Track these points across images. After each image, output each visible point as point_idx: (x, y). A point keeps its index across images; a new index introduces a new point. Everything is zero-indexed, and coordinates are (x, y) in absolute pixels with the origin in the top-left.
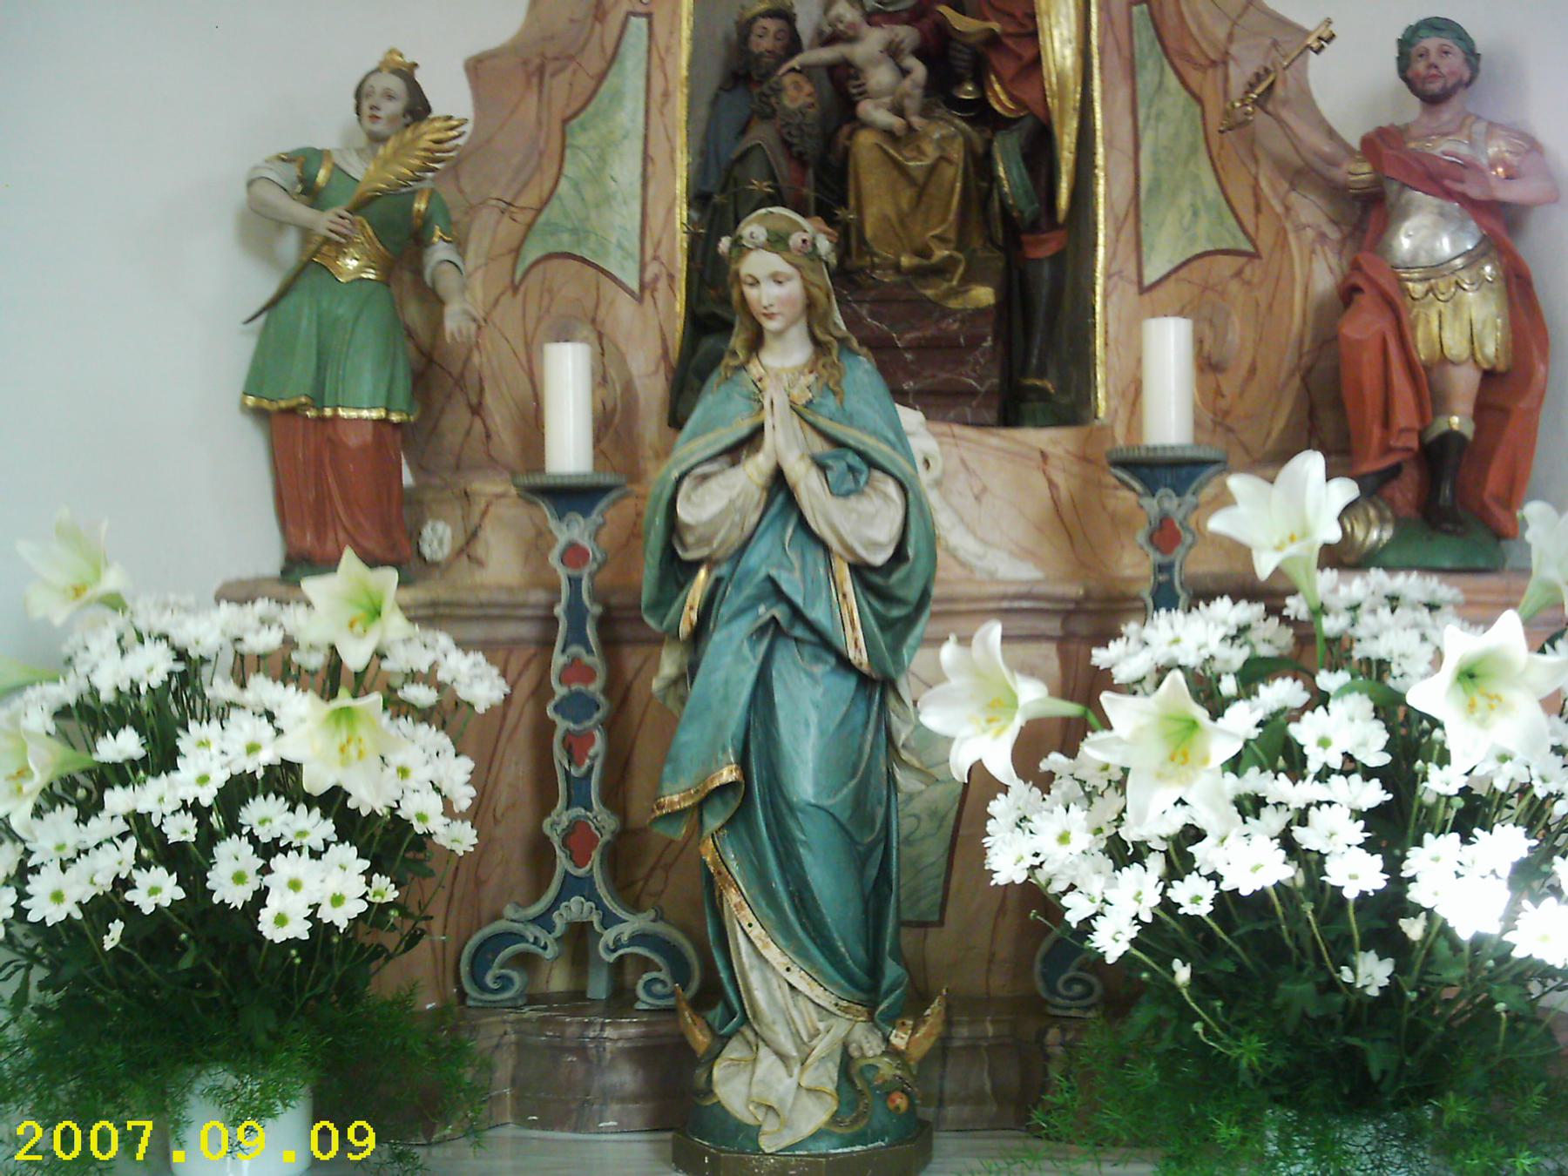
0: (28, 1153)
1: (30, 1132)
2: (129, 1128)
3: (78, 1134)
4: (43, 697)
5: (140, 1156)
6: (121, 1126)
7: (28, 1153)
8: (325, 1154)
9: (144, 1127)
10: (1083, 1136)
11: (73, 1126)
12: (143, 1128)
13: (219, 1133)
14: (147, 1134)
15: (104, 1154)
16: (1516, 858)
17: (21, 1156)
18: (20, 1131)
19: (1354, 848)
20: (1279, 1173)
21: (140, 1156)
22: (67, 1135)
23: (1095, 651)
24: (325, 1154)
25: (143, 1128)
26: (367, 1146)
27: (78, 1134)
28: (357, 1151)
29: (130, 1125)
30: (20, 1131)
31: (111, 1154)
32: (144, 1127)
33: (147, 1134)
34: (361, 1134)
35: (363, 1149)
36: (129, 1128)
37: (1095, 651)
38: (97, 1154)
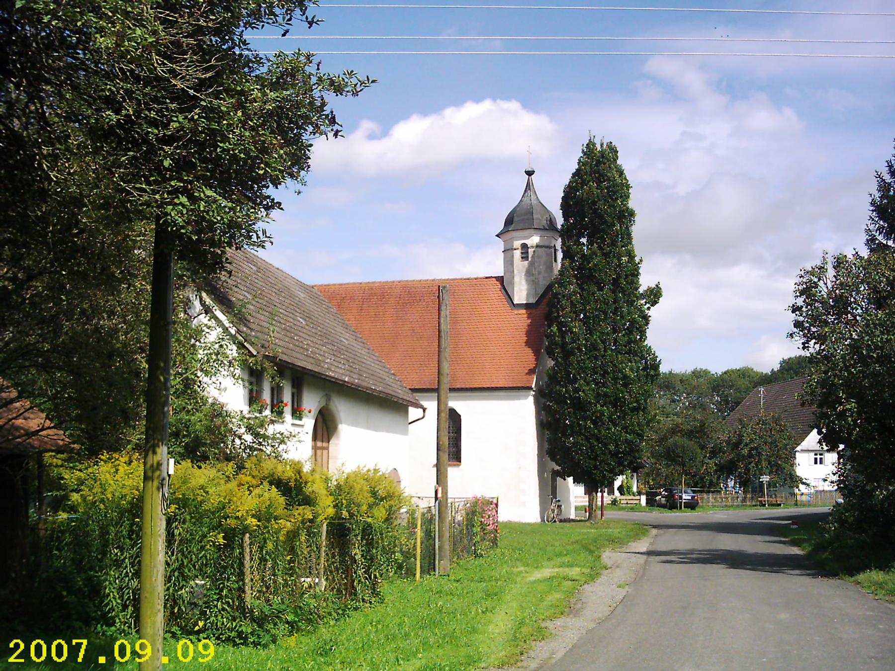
0: (16, 658)
1: (17, 646)
2: (74, 644)
3: (44, 647)
4: (140, 406)
5: (80, 660)
6: (69, 643)
7: (16, 658)
8: (38, 658)
9: (82, 643)
10: (303, 635)
11: (42, 642)
12: (82, 643)
13: (188, 647)
14: (84, 647)
15: (122, 658)
16: (709, 369)
17: (12, 660)
18: (12, 645)
19: (602, 138)
20: (470, 670)
21: (80, 660)
22: (38, 648)
23: (572, 478)
24: (38, 658)
25: (82, 643)
26: (209, 654)
27: (44, 647)
28: (203, 657)
29: (74, 642)
30: (12, 645)
31: (126, 659)
32: (82, 643)
33: (84, 647)
34: (206, 647)
35: (207, 656)
36: (74, 644)
37: (572, 478)
38: (55, 658)
